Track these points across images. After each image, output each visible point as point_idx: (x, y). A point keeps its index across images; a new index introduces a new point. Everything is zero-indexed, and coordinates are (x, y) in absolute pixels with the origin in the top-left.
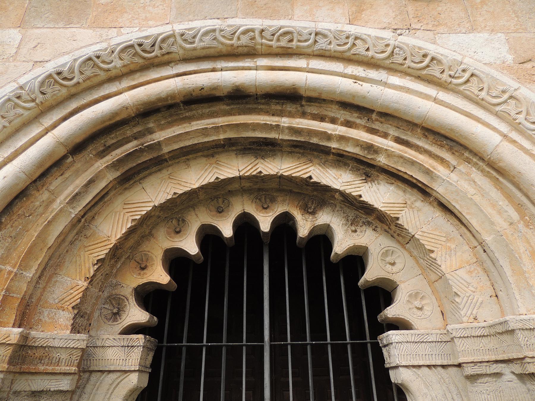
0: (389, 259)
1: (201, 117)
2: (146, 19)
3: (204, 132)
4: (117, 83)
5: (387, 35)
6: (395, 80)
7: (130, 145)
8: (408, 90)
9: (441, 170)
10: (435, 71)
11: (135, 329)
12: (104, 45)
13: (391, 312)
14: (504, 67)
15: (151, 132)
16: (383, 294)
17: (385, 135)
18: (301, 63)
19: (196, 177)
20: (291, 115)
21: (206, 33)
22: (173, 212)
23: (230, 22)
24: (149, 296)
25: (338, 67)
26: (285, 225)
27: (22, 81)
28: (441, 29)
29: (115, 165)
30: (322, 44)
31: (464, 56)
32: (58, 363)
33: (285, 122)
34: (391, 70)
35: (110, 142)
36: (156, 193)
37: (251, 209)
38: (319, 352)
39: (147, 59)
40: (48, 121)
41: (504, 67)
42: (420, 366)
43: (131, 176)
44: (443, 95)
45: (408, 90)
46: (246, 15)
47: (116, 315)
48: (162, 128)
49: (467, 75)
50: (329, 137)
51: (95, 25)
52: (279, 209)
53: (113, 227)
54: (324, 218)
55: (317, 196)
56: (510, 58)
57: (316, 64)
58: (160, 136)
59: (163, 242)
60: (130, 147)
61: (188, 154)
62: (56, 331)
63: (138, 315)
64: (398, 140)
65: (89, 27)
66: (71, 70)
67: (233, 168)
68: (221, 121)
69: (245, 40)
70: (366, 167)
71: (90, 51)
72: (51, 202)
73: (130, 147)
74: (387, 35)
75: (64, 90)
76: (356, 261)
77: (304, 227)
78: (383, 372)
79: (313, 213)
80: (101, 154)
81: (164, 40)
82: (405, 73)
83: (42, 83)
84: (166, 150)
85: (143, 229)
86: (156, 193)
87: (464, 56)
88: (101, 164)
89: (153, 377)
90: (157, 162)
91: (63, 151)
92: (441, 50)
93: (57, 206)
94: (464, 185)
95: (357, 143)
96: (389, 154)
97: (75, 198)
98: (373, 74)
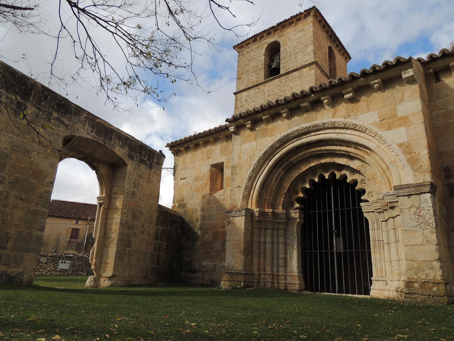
0: (364, 182)
1: (301, 151)
2: (281, 131)
3: (303, 155)
4: (339, 130)
5: (343, 120)
7: (286, 163)
9: (366, 156)
10: (357, 128)
11: (297, 208)
12: (273, 142)
13: (363, 198)
14: (376, 124)
15: (290, 158)
16: (363, 192)
18: (322, 132)
19: (304, 168)
21: (296, 131)
22: (302, 177)
23: (301, 126)
25: (332, 131)
26: (333, 175)
27: (259, 156)
28: (358, 114)
29: (283, 169)
30: (326, 126)
31: (364, 123)
33: (323, 148)
34: (347, 129)
35: (281, 163)
36: (295, 174)
37: (311, 178)
38: (349, 211)
41: (376, 124)
42: (369, 212)
43: (288, 170)
44: (362, 134)
46: (306, 122)
47: (293, 205)
49: (365, 128)
51: (271, 135)
53: (287, 185)
54: (344, 172)
55: (341, 167)
56: (377, 120)
58: (292, 159)
59: (347, 173)
60: (286, 164)
62: (280, 210)
63: (297, 205)
65: (270, 137)
66: (268, 150)
69: (306, 130)
71: (270, 144)
72: (271, 181)
73: (286, 164)
74: (343, 120)
76: (355, 183)
77: (338, 175)
78: (362, 213)
79: (341, 171)
80: (280, 167)
81: (286, 136)
82: (351, 129)
83: (263, 155)
84: (294, 162)
85: (295, 183)
86: (295, 174)
87: (364, 123)
88: (280, 170)
89: (305, 220)
91: (271, 169)
92: (358, 122)
93: (273, 182)
94: (372, 160)
97: (276, 179)
98: (342, 131)
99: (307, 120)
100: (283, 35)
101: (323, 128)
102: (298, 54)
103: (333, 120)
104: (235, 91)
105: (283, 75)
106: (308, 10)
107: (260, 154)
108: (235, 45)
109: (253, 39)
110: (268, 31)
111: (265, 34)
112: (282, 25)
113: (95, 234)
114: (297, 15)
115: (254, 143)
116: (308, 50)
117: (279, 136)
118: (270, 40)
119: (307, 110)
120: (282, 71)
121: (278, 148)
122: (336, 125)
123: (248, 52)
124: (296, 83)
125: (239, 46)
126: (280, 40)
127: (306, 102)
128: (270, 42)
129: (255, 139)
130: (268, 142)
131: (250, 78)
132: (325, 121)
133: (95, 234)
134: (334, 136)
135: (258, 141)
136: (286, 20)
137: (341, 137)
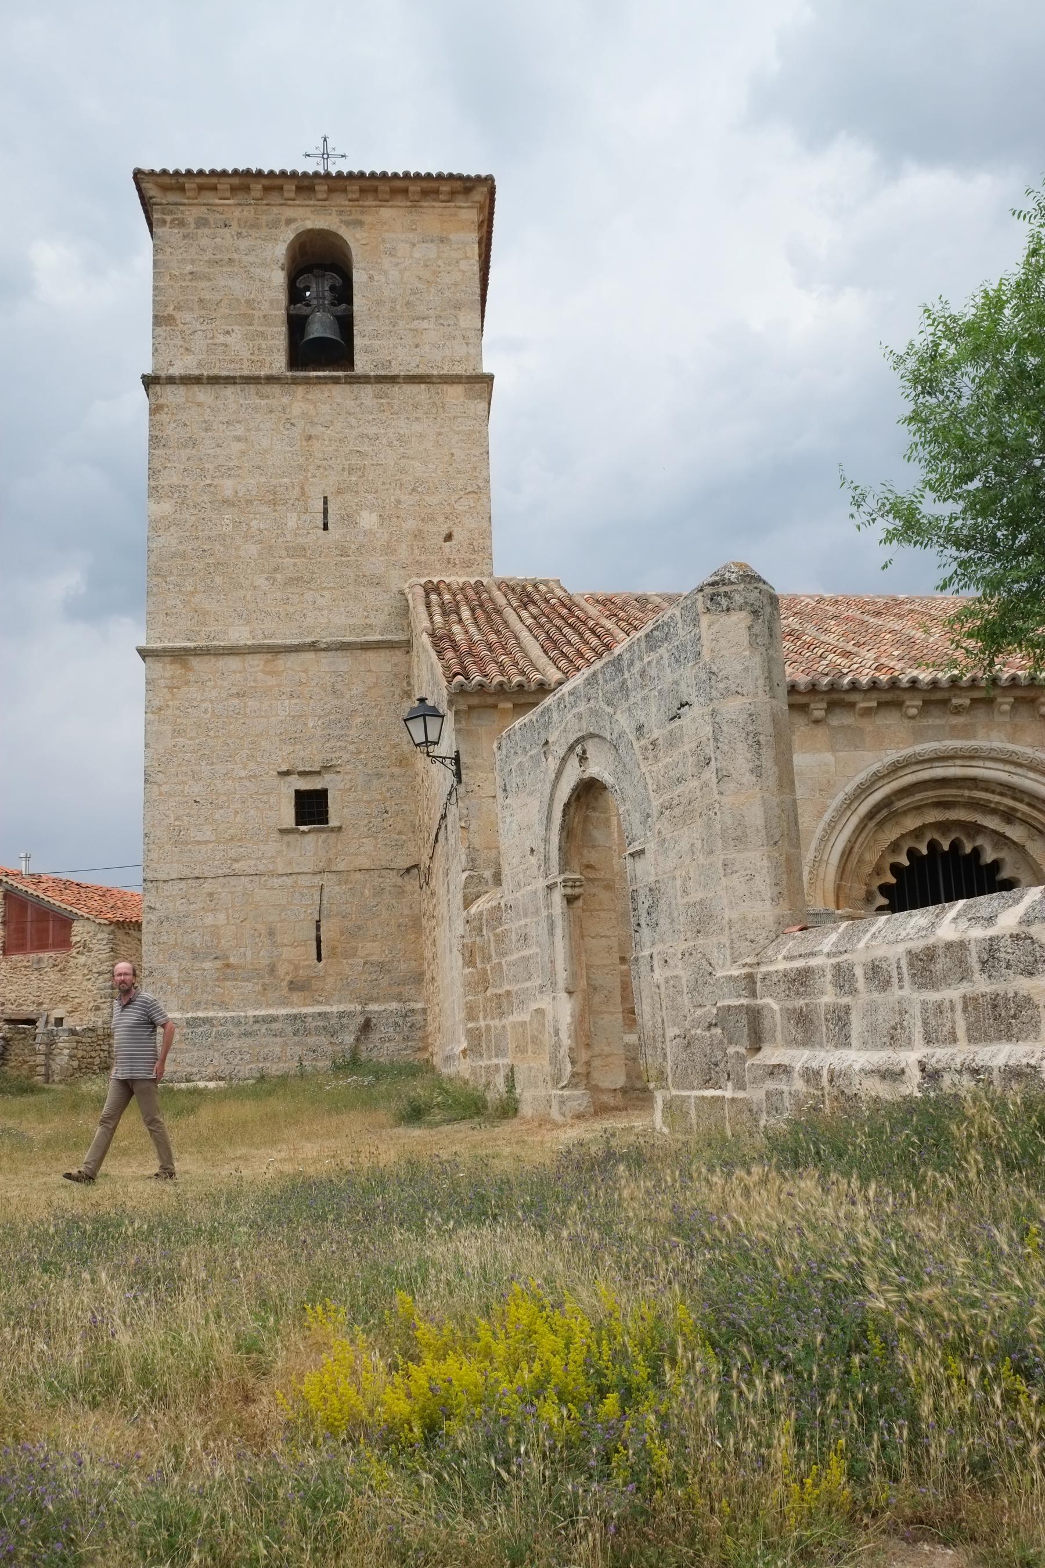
2: (898, 743)
3: (921, 800)
6: (1031, 775)
7: (883, 813)
8: (1037, 781)
17: (1021, 801)
18: (980, 763)
19: (911, 823)
20: (970, 789)
24: (885, 889)
29: (876, 825)
30: (993, 754)
32: (282, 887)
33: (966, 793)
37: (937, 837)
39: (896, 768)
40: (853, 808)
45: (1037, 781)
46: (952, 738)
48: (899, 800)
50: (991, 802)
52: (928, 838)
55: (974, 829)
57: (989, 764)
61: (906, 812)
64: (1029, 805)
67: (933, 816)
68: (930, 793)
70: (1009, 816)
74: (1029, 751)
75: (863, 790)
90: (895, 816)
95: (1006, 806)
96: (1023, 813)
98: (1019, 771)
99: (956, 732)
100: (360, 223)
101: (973, 756)
102: (425, 324)
103: (1011, 747)
104: (148, 371)
105: (365, 379)
106: (469, 178)
107: (850, 787)
108: (146, 167)
109: (236, 181)
110: (306, 183)
111: (290, 187)
112: (365, 184)
113: (487, 991)
114: (429, 176)
115: (828, 757)
116: (463, 324)
117: (893, 755)
118: (312, 218)
119: (958, 711)
120: (362, 364)
121: (883, 777)
122: (1015, 758)
123: (202, 223)
124: (417, 427)
125: (167, 180)
126: (357, 243)
127: (966, 697)
128: (309, 225)
129: (833, 749)
130: (871, 761)
131: (221, 339)
132: (996, 745)
133: (487, 991)
134: (1003, 776)
135: (841, 754)
136: (384, 174)
137: (1015, 780)
